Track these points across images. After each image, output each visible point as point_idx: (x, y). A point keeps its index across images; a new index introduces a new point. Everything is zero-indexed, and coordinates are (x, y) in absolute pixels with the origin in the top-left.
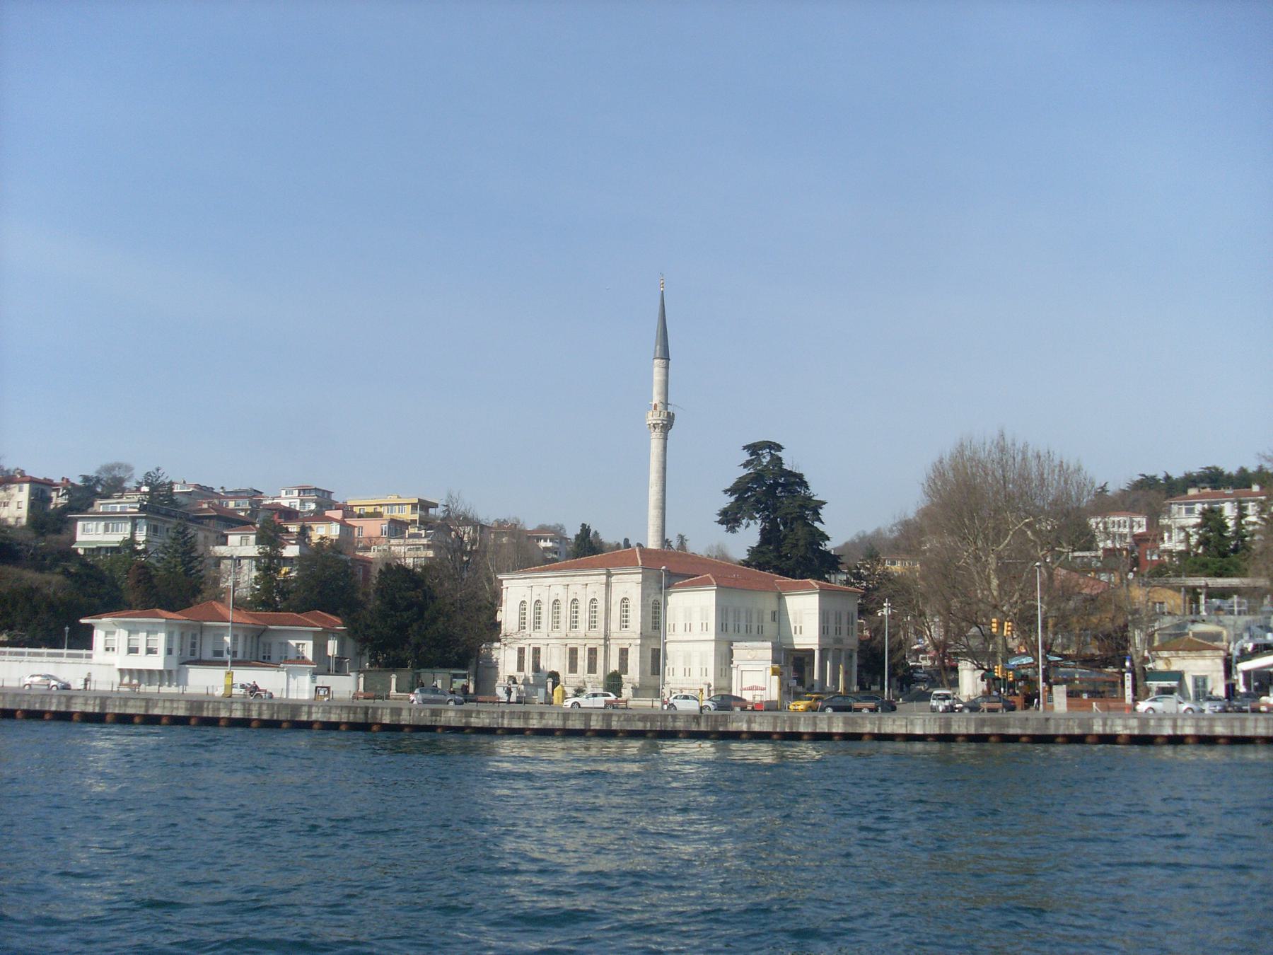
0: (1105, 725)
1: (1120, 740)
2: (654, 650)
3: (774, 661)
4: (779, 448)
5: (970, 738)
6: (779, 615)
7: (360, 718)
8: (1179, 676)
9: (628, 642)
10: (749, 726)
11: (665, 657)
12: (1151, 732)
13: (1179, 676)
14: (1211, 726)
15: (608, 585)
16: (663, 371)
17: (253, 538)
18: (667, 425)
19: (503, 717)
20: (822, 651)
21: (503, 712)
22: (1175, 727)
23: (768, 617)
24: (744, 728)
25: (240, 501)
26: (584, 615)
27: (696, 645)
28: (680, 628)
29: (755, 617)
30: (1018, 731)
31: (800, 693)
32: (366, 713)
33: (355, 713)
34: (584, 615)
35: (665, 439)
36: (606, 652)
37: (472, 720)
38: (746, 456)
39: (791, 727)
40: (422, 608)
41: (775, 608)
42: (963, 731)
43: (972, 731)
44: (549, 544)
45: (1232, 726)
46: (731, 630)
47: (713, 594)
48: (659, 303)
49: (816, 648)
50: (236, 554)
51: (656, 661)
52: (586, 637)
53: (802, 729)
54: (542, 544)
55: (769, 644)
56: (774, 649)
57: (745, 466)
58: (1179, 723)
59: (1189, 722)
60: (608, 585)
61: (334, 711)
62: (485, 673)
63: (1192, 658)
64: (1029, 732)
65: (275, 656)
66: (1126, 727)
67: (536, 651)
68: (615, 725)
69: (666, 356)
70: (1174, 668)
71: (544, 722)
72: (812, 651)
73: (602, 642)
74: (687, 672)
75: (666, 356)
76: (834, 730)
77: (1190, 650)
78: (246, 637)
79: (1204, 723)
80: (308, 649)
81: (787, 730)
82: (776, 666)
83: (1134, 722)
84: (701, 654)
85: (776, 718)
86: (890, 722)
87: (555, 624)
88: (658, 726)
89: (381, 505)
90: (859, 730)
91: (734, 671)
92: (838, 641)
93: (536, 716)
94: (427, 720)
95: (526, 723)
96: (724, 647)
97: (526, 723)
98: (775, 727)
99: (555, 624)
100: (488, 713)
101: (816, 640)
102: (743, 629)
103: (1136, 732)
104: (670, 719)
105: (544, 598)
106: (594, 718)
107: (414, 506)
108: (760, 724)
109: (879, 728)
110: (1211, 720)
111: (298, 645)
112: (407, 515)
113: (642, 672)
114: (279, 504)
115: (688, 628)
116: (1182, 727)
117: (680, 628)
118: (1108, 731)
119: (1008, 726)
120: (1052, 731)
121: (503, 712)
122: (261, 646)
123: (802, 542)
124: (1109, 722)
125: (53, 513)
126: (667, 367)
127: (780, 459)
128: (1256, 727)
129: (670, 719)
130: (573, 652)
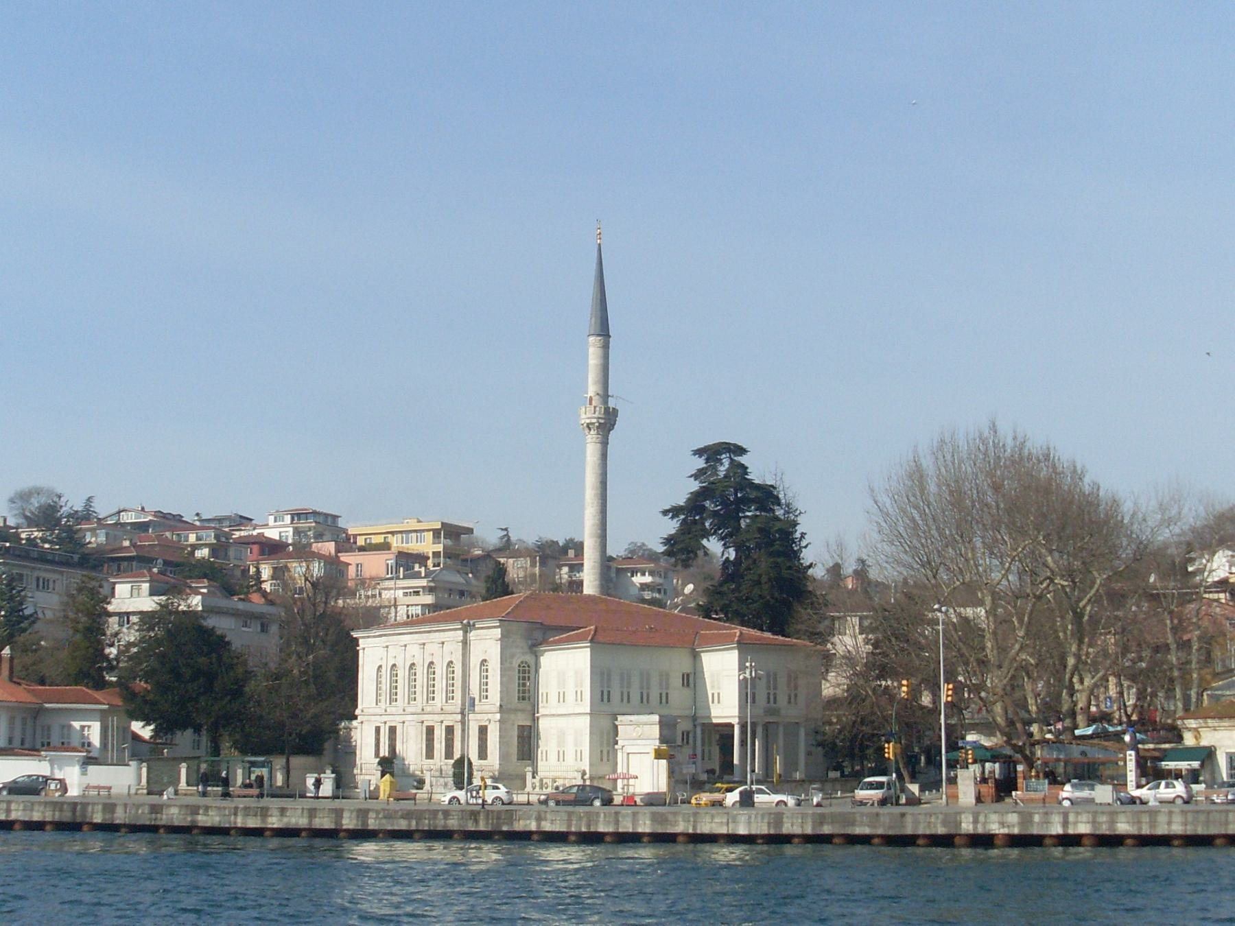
0: (976, 822)
1: (997, 842)
2: (521, 728)
3: (663, 739)
4: (741, 451)
5: (808, 839)
6: (693, 680)
7: (67, 816)
8: (1207, 755)
9: (486, 717)
10: (539, 825)
11: (538, 738)
12: (1035, 831)
13: (1207, 755)
14: (1113, 822)
15: (465, 643)
16: (599, 352)
17: (146, 586)
18: (607, 423)
19: (236, 814)
20: (743, 727)
21: (236, 808)
22: (1065, 823)
23: (676, 681)
24: (533, 826)
25: (203, 533)
26: (440, 684)
27: (570, 719)
28: (553, 698)
29: (654, 682)
30: (866, 831)
31: (704, 783)
32: (74, 811)
33: (61, 810)
34: (440, 684)
35: (605, 443)
36: (463, 730)
37: (200, 818)
38: (700, 463)
39: (589, 826)
40: (211, 677)
41: (686, 667)
42: (797, 830)
43: (809, 830)
44: (648, 579)
45: (1139, 822)
46: (610, 700)
47: (736, 652)
48: (596, 255)
49: (735, 721)
50: (125, 608)
51: (526, 744)
52: (386, 713)
53: (601, 829)
54: (638, 579)
55: (656, 718)
56: (662, 724)
57: (696, 476)
58: (1071, 818)
59: (1084, 817)
60: (465, 643)
61: (36, 808)
62: (342, 761)
63: (1226, 728)
64: (880, 831)
65: (55, 740)
66: (1002, 824)
67: (393, 730)
68: (372, 824)
69: (604, 331)
70: (1204, 743)
71: (285, 820)
72: (731, 726)
73: (459, 717)
74: (561, 756)
75: (604, 331)
76: (640, 830)
77: (1221, 718)
78: (24, 720)
79: (1103, 819)
80: (94, 732)
81: (584, 829)
82: (664, 747)
83: (1013, 818)
84: (580, 731)
85: (570, 814)
86: (708, 819)
87: (412, 698)
88: (426, 825)
89: (393, 533)
90: (670, 830)
91: (619, 754)
92: (771, 712)
93: (276, 812)
94: (145, 818)
95: (264, 821)
96: (605, 723)
97: (264, 821)
98: (569, 825)
99: (412, 698)
100: (219, 808)
101: (736, 712)
102: (635, 697)
103: (1016, 831)
104: (440, 816)
105: (400, 664)
106: (346, 814)
107: (436, 533)
108: (552, 822)
109: (694, 827)
110: (1113, 815)
111: (83, 727)
112: (427, 546)
113: (504, 757)
114: (262, 534)
115: (562, 698)
116: (1076, 823)
117: (553, 698)
118: (980, 830)
119: (853, 824)
120: (909, 831)
121: (236, 808)
122: (39, 731)
123: (764, 579)
124: (982, 818)
125: (69, 548)
126: (606, 347)
127: (744, 468)
128: (1169, 823)
129: (440, 816)
130: (430, 731)
